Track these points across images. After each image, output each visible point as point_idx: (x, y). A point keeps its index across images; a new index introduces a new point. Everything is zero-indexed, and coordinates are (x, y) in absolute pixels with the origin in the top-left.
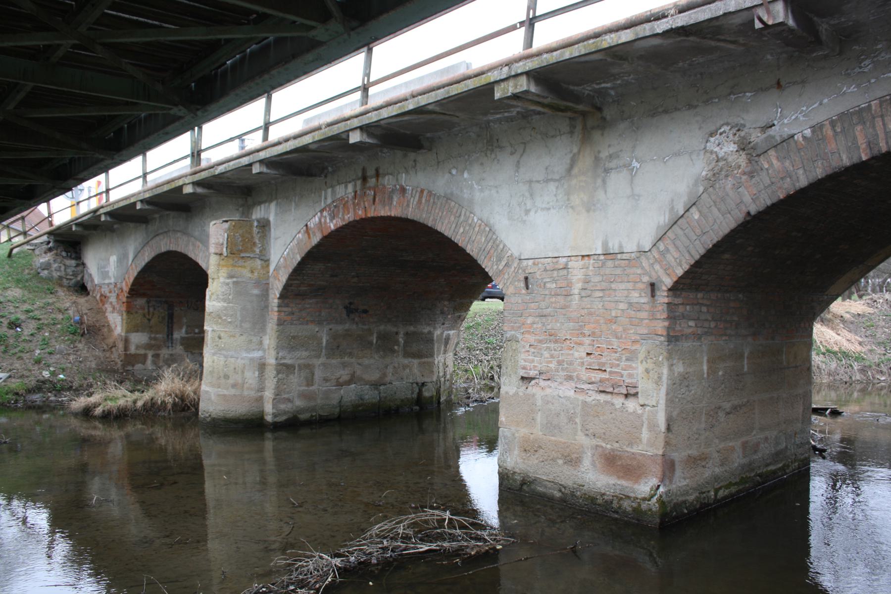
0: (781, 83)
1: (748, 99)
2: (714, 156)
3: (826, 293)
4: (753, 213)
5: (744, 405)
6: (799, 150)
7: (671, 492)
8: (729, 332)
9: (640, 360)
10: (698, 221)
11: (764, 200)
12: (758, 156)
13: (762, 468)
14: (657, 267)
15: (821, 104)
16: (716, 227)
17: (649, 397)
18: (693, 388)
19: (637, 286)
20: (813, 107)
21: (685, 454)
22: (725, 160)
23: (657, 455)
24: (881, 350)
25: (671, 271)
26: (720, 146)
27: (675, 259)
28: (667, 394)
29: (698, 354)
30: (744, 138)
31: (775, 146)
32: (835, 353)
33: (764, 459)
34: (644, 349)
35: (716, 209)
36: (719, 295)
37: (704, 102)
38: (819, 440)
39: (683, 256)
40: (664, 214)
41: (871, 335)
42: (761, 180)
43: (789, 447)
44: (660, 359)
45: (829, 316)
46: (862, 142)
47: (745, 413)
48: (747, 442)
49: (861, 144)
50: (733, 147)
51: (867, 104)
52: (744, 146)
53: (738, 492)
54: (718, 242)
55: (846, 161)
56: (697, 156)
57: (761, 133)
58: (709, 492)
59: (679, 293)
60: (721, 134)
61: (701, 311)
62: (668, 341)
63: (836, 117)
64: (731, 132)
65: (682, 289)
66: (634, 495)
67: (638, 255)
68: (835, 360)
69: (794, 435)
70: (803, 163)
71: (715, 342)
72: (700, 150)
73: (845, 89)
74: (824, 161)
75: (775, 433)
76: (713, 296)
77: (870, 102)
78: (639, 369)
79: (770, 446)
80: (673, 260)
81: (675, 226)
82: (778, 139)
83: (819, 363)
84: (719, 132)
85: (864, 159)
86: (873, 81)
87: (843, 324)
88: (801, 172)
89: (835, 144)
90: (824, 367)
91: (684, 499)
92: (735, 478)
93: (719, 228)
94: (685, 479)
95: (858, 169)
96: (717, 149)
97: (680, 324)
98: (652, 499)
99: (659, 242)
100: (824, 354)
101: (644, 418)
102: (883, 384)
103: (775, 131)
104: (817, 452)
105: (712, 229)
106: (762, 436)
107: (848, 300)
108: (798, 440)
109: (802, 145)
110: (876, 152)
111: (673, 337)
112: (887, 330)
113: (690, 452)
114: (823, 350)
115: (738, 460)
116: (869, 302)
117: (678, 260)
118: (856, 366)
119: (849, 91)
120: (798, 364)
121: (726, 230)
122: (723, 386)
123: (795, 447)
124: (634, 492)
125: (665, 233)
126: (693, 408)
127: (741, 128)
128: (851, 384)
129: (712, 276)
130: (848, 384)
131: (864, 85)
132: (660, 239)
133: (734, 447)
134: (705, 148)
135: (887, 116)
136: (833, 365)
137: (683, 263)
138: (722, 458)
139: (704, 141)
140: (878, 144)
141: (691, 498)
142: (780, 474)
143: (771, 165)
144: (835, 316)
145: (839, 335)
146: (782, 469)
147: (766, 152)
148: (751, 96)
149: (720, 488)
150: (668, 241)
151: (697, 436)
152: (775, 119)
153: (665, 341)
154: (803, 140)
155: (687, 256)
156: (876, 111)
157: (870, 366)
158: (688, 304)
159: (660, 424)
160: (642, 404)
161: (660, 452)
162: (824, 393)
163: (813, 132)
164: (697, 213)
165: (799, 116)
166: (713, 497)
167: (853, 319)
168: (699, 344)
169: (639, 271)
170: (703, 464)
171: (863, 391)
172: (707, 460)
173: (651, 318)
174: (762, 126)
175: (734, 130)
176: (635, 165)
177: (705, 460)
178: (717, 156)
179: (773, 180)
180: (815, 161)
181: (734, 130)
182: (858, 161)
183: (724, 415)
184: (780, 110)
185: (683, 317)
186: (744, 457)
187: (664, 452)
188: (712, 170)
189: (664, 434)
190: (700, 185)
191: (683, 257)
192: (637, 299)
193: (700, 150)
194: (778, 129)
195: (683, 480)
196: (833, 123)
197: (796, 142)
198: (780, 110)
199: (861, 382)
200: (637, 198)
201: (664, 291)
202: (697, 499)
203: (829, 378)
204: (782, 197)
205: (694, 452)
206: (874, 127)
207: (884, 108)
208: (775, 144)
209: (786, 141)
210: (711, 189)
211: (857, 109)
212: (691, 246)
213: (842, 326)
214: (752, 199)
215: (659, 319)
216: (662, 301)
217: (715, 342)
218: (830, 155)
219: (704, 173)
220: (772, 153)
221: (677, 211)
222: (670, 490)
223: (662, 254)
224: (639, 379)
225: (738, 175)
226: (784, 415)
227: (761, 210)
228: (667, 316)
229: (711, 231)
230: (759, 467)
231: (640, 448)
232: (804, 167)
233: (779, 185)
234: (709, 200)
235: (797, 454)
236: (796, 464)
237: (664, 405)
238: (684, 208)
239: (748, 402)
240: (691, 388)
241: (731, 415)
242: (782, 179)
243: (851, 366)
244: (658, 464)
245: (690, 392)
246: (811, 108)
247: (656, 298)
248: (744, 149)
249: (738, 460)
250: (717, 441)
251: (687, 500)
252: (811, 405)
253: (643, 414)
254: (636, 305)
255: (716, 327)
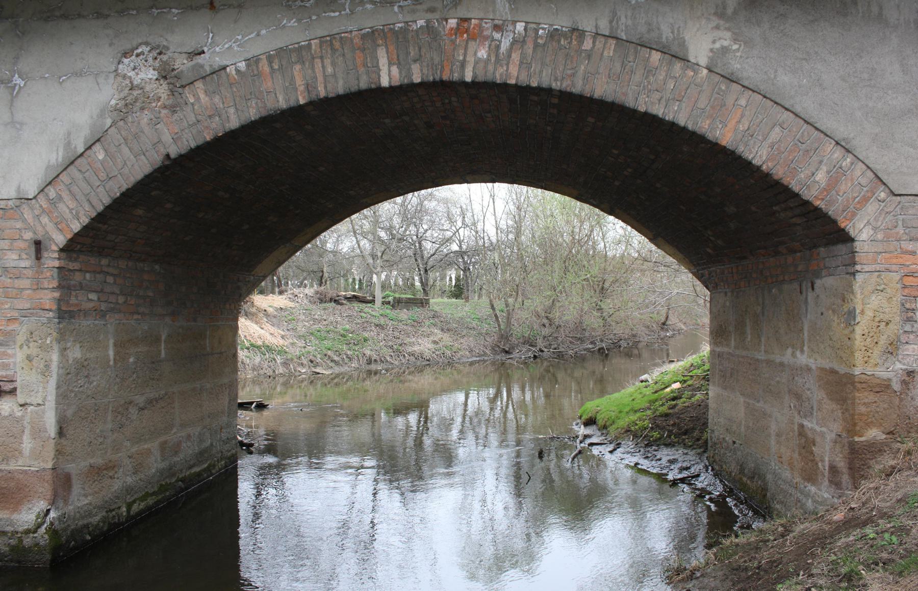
0: (215, 4)
1: (174, 17)
2: (128, 82)
3: (253, 273)
4: (173, 156)
5: (161, 398)
6: (231, 84)
7: (66, 516)
8: (141, 310)
9: (19, 344)
10: (102, 162)
11: (188, 141)
12: (183, 87)
13: (184, 471)
14: (45, 220)
15: (258, 35)
16: (126, 171)
17: (32, 394)
18: (95, 379)
19: (15, 244)
20: (250, 37)
21: (84, 464)
22: (141, 89)
23: (44, 469)
24: (301, 343)
25: (64, 225)
26: (136, 71)
27: (71, 210)
28: (58, 387)
29: (102, 336)
30: (165, 63)
31: (203, 78)
32: (259, 347)
33: (186, 461)
34: (24, 329)
35: (127, 149)
36: (130, 264)
37: (117, 12)
38: (245, 435)
39: (81, 206)
40: (57, 150)
41: (293, 329)
42: (185, 116)
43: (214, 444)
44: (48, 342)
45: (254, 310)
46: (300, 83)
47: (163, 408)
48: (165, 442)
49: (299, 86)
50: (152, 74)
51: (307, 43)
52: (166, 74)
53: (157, 503)
54: (128, 190)
55: (282, 102)
56: (105, 79)
57: (187, 60)
58: (119, 508)
59: (75, 255)
60: (138, 55)
61: (105, 282)
62: (59, 318)
63: (274, 52)
64: (151, 55)
65: (80, 251)
66: (12, 529)
67: (18, 203)
68: (259, 355)
69: (219, 430)
70: (234, 100)
71: (125, 321)
72: (109, 72)
73: (285, 21)
74: (259, 101)
75: (199, 429)
76: (123, 264)
77: (310, 40)
78: (18, 356)
79: (193, 445)
80: (68, 211)
81: (72, 167)
82: (208, 70)
83: (244, 357)
84: (135, 52)
85: (301, 103)
86: (314, 18)
87: (267, 318)
88: (232, 110)
89: (271, 82)
90: (248, 361)
91: (85, 522)
92: (153, 487)
93: (130, 173)
94: (86, 496)
95: (295, 113)
96: (131, 74)
97: (76, 296)
98: (39, 530)
99: (49, 187)
100: (248, 348)
101: (25, 422)
102: (304, 376)
103: (205, 59)
104: (244, 448)
105: (120, 173)
106: (183, 434)
107: (271, 295)
108: (224, 436)
109: (235, 79)
110: (314, 97)
111: (66, 312)
112: (307, 324)
113: (92, 461)
114: (247, 344)
115: (155, 464)
116: (291, 296)
117: (74, 212)
118: (279, 359)
119: (289, 25)
120: (223, 350)
121: (139, 176)
122: (135, 376)
123: (222, 443)
124: (12, 524)
125: (58, 176)
126: (96, 404)
127: (163, 51)
128: (274, 378)
129: (120, 237)
130: (271, 377)
131: (305, 21)
132: (50, 183)
133: (150, 450)
134: (116, 71)
135: (326, 58)
136: (257, 360)
137: (80, 215)
138: (135, 464)
139: (116, 61)
140: (316, 88)
141: (95, 520)
142: (205, 475)
143: (198, 99)
144: (259, 310)
145: (262, 328)
146: (208, 469)
147: (192, 83)
148: (178, 13)
149: (134, 502)
150: (62, 187)
151: (101, 440)
152: (206, 46)
153: (54, 318)
154: (236, 74)
155: (87, 207)
156: (315, 51)
157: (292, 359)
158: (87, 272)
159: (48, 427)
160: (23, 403)
161: (50, 465)
162: (248, 389)
163: (248, 66)
164: (102, 151)
165: (234, 45)
166: (124, 514)
167: (276, 313)
168: (103, 323)
169: (19, 225)
170: (111, 474)
171: (286, 384)
172: (116, 469)
173: (35, 287)
174: (190, 52)
175: (155, 53)
176: (18, 82)
177: (113, 469)
178: (131, 82)
179: (199, 118)
180: (249, 99)
181: (155, 53)
182: (295, 105)
183: (137, 412)
184: (211, 35)
185: (81, 287)
186: (163, 461)
187: (54, 465)
188: (124, 98)
189: (55, 440)
190: (107, 116)
191: (81, 208)
192: (17, 262)
193: (109, 72)
194: (207, 57)
195: (83, 498)
196: (270, 59)
197: (228, 76)
198: (211, 35)
199: (284, 375)
200: (18, 126)
201: (54, 251)
202: (104, 520)
203: (253, 373)
204: (208, 139)
205: (98, 461)
206: (313, 68)
207: (324, 49)
208: (204, 75)
209: (217, 73)
210: (121, 123)
211: (296, 46)
212: (93, 194)
213: (265, 320)
214: (173, 139)
215: (46, 289)
216: (50, 266)
217: (125, 321)
218: (265, 94)
219: (113, 102)
220: (199, 85)
221: (75, 148)
222: (65, 514)
223: (52, 202)
224: (17, 370)
225: (156, 109)
226: (208, 409)
227: (183, 152)
228: (57, 284)
229: (119, 175)
230: (181, 470)
231: (20, 463)
232: (236, 105)
233: (206, 124)
234: (119, 136)
235: (224, 451)
236: (223, 462)
237: (54, 402)
238: (85, 145)
239: (166, 394)
240: (92, 378)
241: (146, 411)
242: (210, 117)
243: (275, 359)
244: (47, 482)
245: (91, 383)
246: (247, 38)
247: (43, 260)
248: (165, 78)
249: (155, 465)
250: (128, 444)
251: (91, 523)
252: (237, 400)
253: (23, 416)
254: (14, 271)
255: (125, 302)
